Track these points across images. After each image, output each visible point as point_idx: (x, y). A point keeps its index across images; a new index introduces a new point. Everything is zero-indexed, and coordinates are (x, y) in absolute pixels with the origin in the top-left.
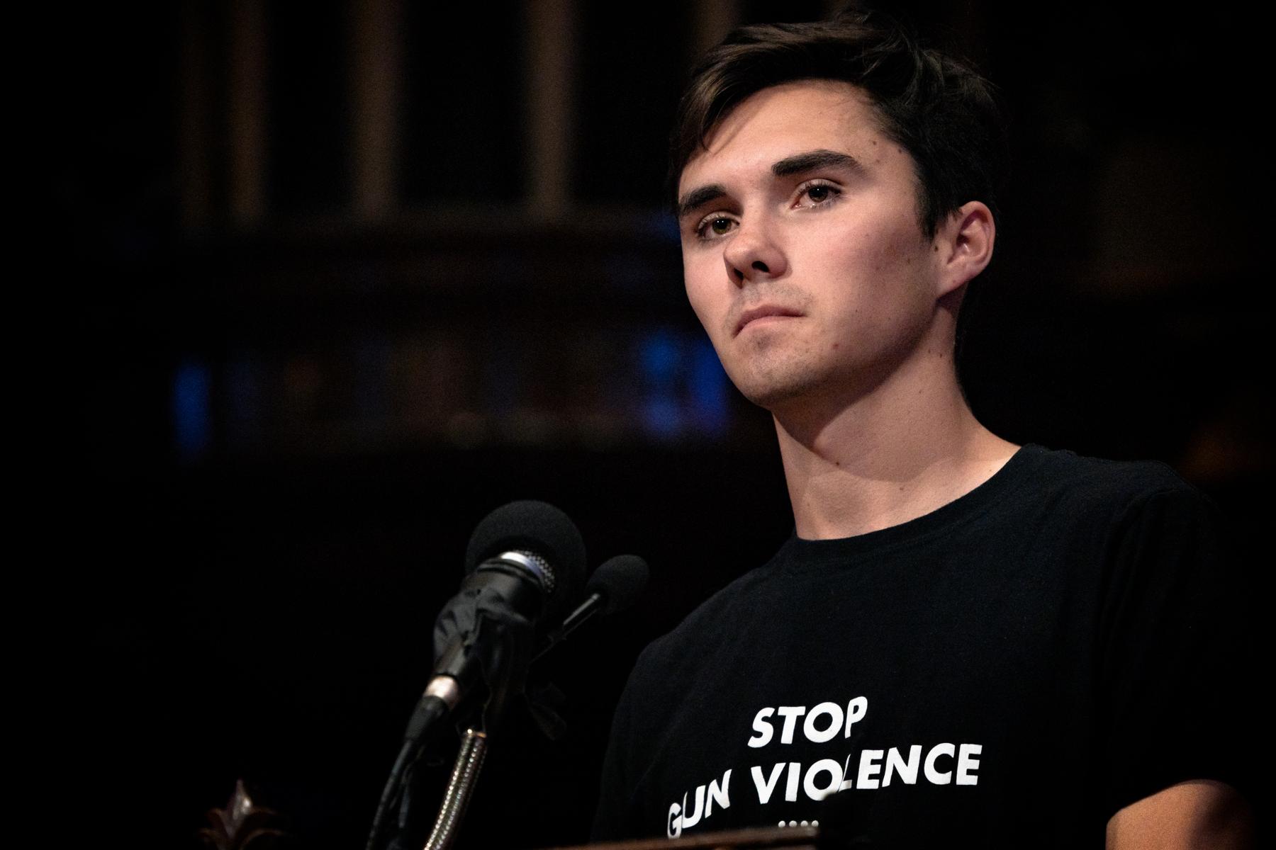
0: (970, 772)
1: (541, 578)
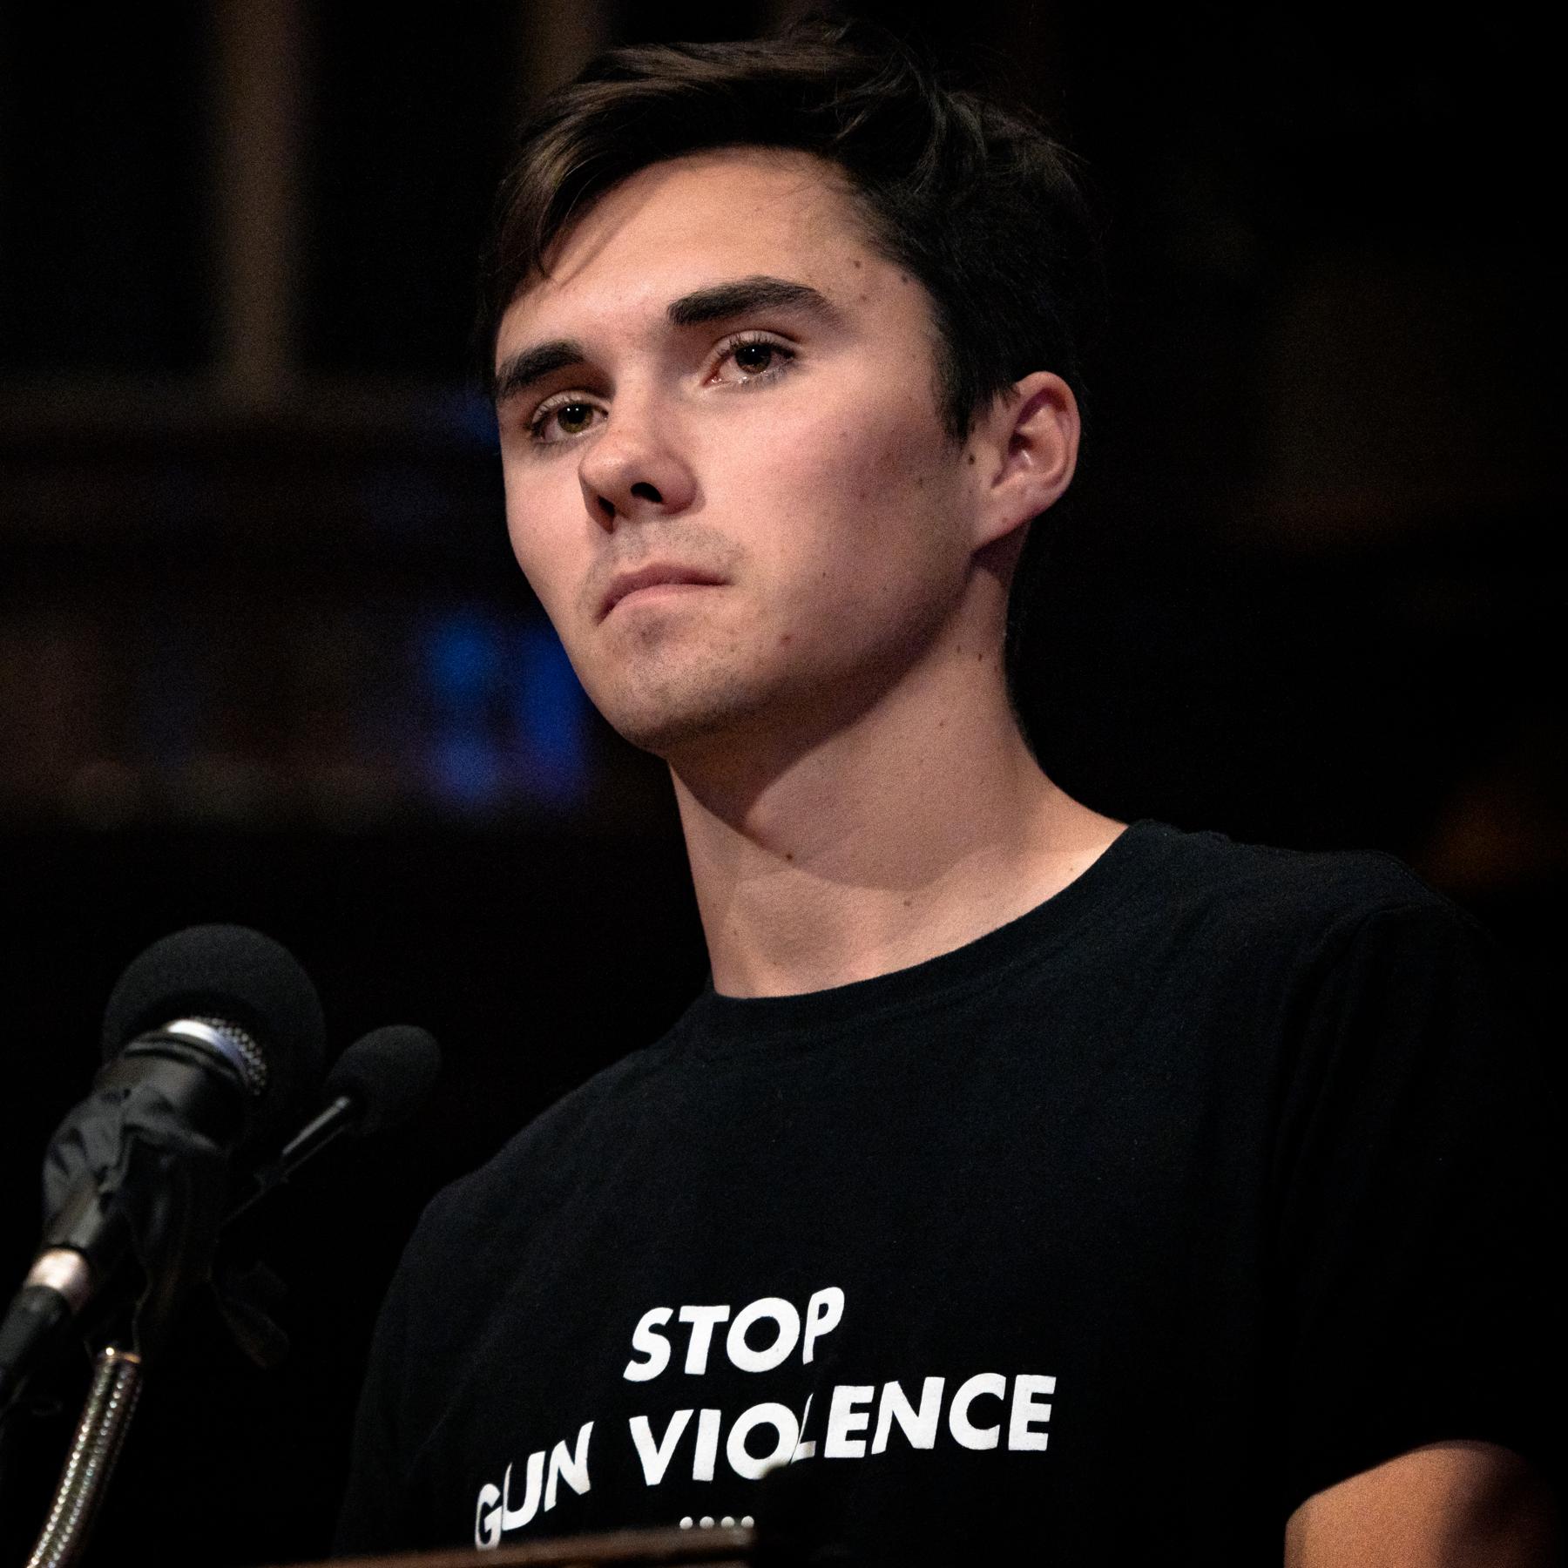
0: (1034, 1427)
1: (241, 1067)
